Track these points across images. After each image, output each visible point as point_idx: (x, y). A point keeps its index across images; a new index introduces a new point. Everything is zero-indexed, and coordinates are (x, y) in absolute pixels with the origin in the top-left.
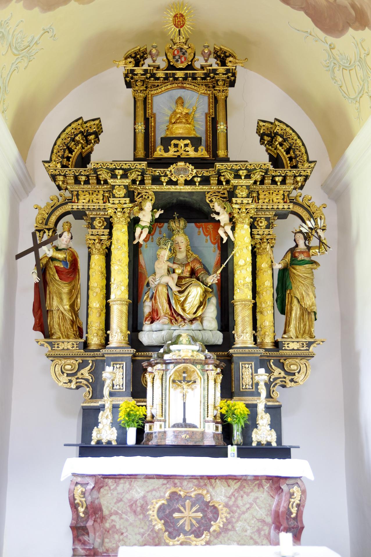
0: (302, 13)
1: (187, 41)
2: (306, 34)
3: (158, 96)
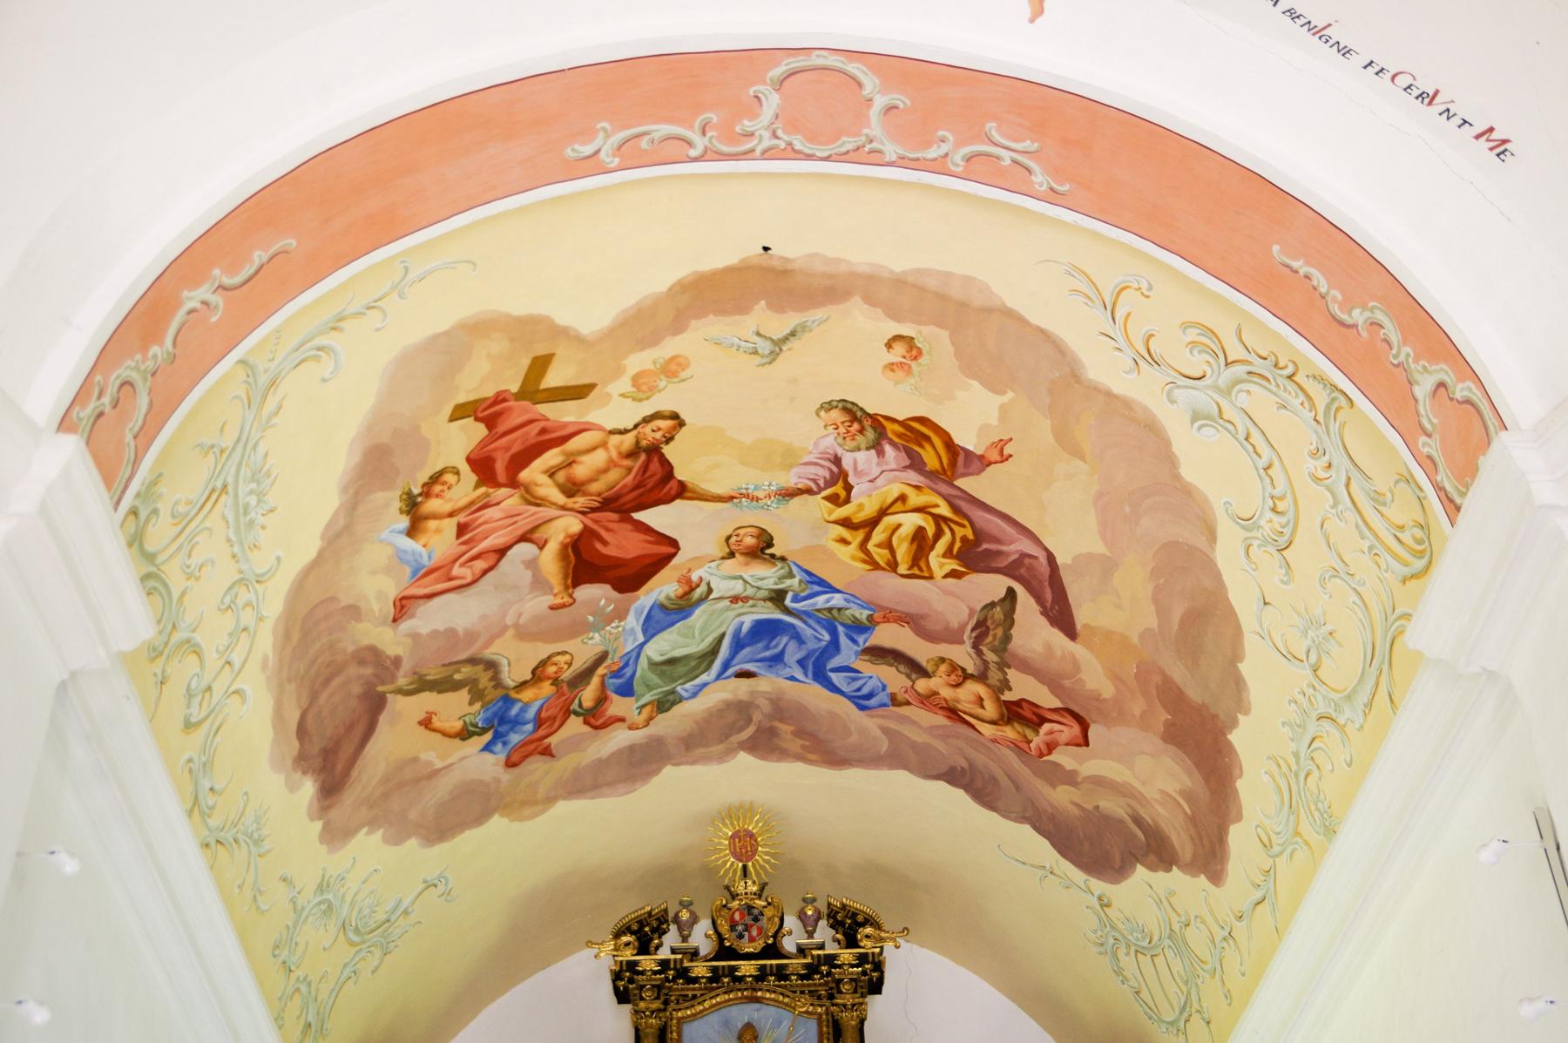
0: (1027, 828)
1: (762, 889)
2: (1041, 872)
3: (695, 1024)
